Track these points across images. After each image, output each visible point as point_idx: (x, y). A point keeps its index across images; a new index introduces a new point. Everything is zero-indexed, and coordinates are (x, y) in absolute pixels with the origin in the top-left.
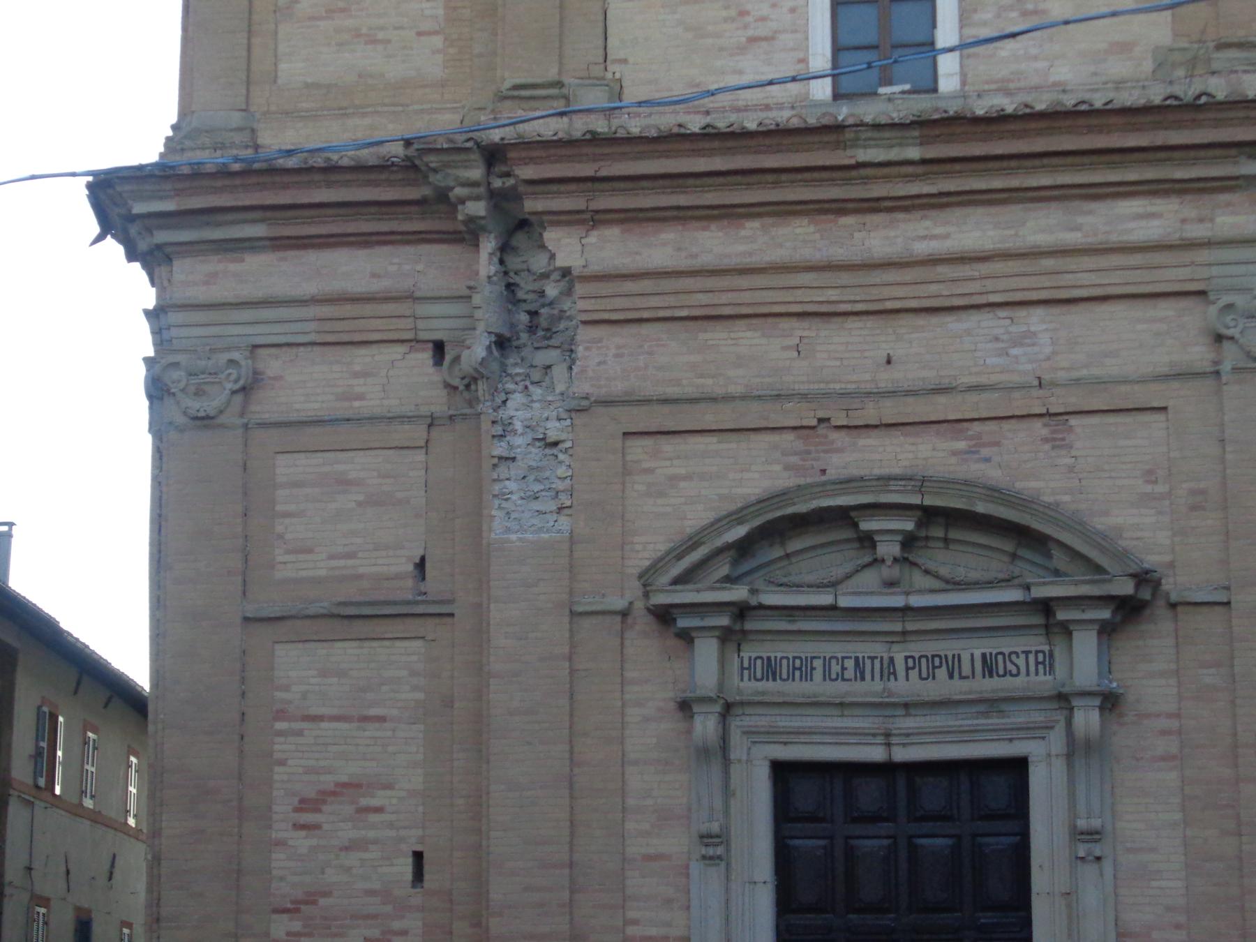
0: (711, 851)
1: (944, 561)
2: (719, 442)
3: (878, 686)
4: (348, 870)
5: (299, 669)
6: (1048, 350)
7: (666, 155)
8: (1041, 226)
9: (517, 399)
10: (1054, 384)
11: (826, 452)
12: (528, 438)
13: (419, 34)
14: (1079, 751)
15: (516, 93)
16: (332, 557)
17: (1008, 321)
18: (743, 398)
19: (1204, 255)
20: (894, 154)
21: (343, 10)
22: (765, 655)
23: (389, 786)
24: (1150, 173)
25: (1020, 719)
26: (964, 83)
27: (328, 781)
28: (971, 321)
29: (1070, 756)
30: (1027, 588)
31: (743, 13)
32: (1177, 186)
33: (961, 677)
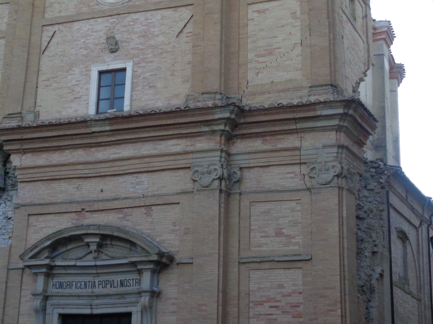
2: (55, 217)
3: (90, 290)
6: (146, 186)
7: (41, 131)
8: (146, 149)
10: (147, 197)
11: (84, 219)
12: (4, 216)
17: (136, 178)
18: (61, 203)
19: (190, 156)
20: (103, 129)
22: (59, 281)
24: (175, 132)
25: (128, 300)
28: (126, 178)
31: (73, 91)
32: (185, 135)
33: (114, 287)
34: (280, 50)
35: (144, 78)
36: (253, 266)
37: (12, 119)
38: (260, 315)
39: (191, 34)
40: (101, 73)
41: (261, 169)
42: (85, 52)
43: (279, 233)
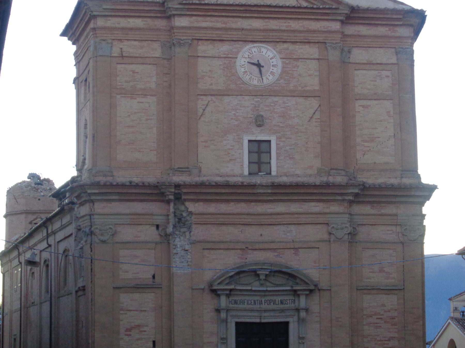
0: (223, 342)
1: (272, 279)
3: (258, 306)
4: (138, 345)
5: (126, 299)
8: (294, 208)
9: (177, 240)
10: (296, 242)
12: (181, 248)
13: (151, 150)
14: (301, 321)
15: (179, 170)
16: (133, 274)
20: (265, 191)
21: (132, 143)
23: (147, 326)
26: (277, 173)
27: (133, 325)
29: (298, 321)
30: (292, 287)
31: (229, 153)
34: (379, 139)
35: (285, 150)
36: (365, 291)
37: (183, 173)
38: (370, 323)
39: (319, 120)
40: (250, 141)
41: (370, 226)
42: (236, 123)
43: (381, 271)
